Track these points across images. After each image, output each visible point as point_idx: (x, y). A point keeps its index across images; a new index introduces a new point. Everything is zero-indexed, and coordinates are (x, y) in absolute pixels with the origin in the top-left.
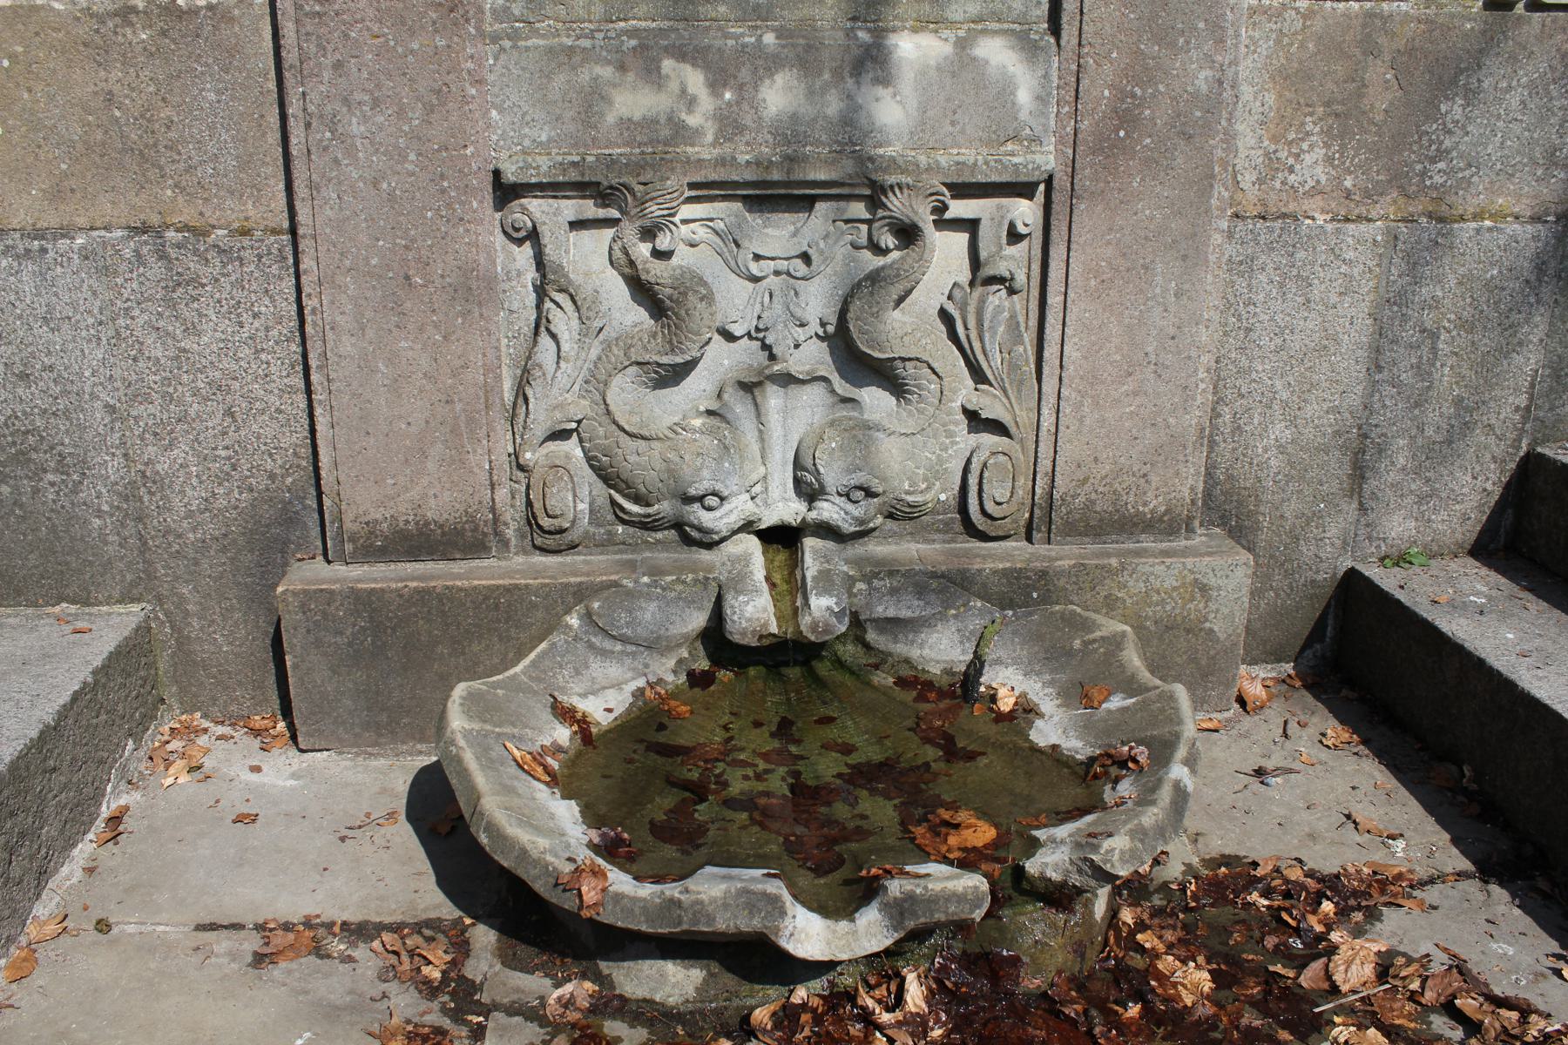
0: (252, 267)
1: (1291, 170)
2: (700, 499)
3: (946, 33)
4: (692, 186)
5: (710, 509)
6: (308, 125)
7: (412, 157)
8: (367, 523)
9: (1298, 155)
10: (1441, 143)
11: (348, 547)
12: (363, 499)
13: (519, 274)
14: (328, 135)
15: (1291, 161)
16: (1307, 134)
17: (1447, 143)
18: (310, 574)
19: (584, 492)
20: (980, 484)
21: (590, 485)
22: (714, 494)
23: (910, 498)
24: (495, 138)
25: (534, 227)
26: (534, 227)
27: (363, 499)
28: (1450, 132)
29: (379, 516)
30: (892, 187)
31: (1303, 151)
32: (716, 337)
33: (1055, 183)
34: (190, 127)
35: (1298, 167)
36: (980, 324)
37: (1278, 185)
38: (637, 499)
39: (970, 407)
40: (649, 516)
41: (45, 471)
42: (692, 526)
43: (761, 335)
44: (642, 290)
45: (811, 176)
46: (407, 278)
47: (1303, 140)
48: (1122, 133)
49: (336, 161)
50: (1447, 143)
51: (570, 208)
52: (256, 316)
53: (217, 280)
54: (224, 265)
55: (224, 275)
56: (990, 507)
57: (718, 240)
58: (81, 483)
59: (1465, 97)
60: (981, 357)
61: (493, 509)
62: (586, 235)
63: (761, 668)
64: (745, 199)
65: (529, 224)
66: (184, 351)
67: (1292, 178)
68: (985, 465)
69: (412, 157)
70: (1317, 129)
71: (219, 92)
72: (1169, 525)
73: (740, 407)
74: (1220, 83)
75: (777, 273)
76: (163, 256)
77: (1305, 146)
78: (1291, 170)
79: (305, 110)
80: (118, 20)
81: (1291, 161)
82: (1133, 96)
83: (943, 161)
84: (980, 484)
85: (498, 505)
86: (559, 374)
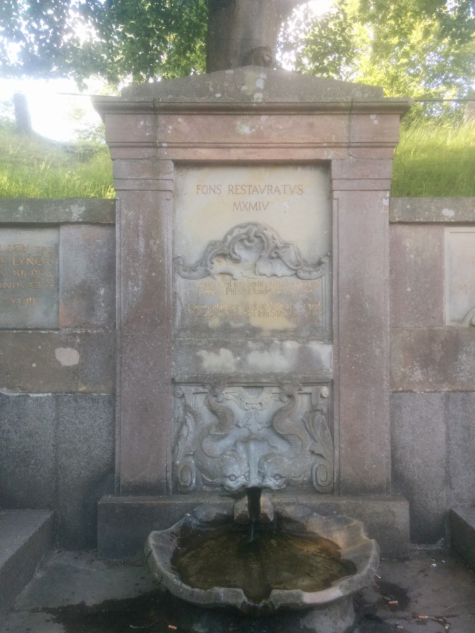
0: (101, 404)
1: (411, 377)
2: (229, 477)
3: (300, 340)
4: (228, 383)
5: (232, 480)
6: (121, 365)
7: (150, 374)
8: (128, 483)
9: (413, 372)
10: (460, 368)
11: (121, 490)
12: (126, 475)
13: (178, 407)
14: (127, 368)
15: (410, 374)
16: (415, 366)
17: (462, 368)
18: (107, 499)
19: (194, 474)
20: (316, 474)
21: (196, 472)
22: (233, 475)
23: (294, 479)
24: (173, 369)
25: (183, 395)
26: (183, 395)
27: (126, 475)
28: (463, 365)
29: (131, 481)
30: (285, 384)
31: (414, 371)
32: (235, 427)
33: (334, 382)
34: (88, 364)
35: (413, 376)
36: (313, 424)
37: (407, 381)
38: (211, 477)
39: (312, 450)
40: (214, 482)
41: (30, 464)
42: (227, 486)
43: (248, 426)
44: (213, 412)
45: (262, 381)
46: (146, 408)
47: (414, 368)
48: (353, 368)
49: (129, 375)
50: (462, 368)
51: (193, 389)
52: (101, 418)
53: (90, 408)
54: (93, 403)
55: (92, 406)
56: (319, 482)
57: (236, 399)
58: (40, 468)
59: (467, 354)
60: (314, 434)
61: (166, 479)
62: (198, 396)
63: (375, 116)
64: (243, 387)
65: (182, 394)
66: (78, 428)
67: (411, 379)
68: (317, 468)
69: (150, 374)
70: (418, 364)
71: (97, 356)
72: (377, 491)
73: (241, 448)
74: (383, 352)
75: (252, 408)
76: (76, 401)
77: (414, 369)
78: (411, 377)
79: (121, 361)
80: (72, 336)
81: (410, 374)
82: (356, 357)
83: (300, 377)
84: (316, 474)
85: (168, 478)
86: (188, 437)
